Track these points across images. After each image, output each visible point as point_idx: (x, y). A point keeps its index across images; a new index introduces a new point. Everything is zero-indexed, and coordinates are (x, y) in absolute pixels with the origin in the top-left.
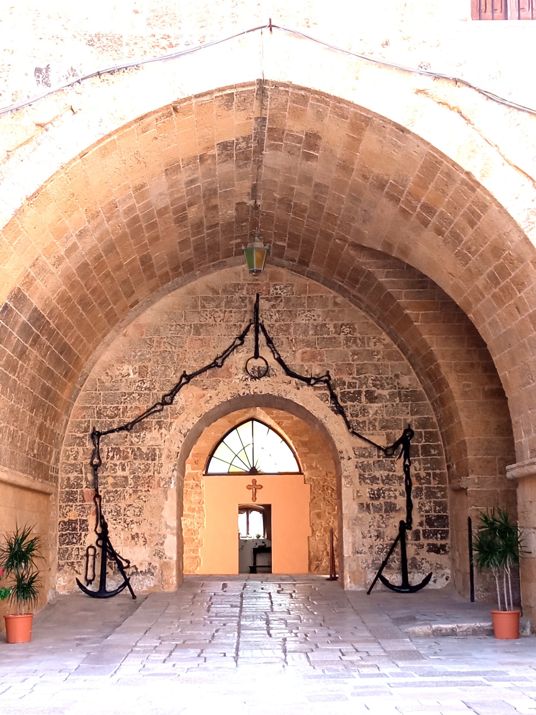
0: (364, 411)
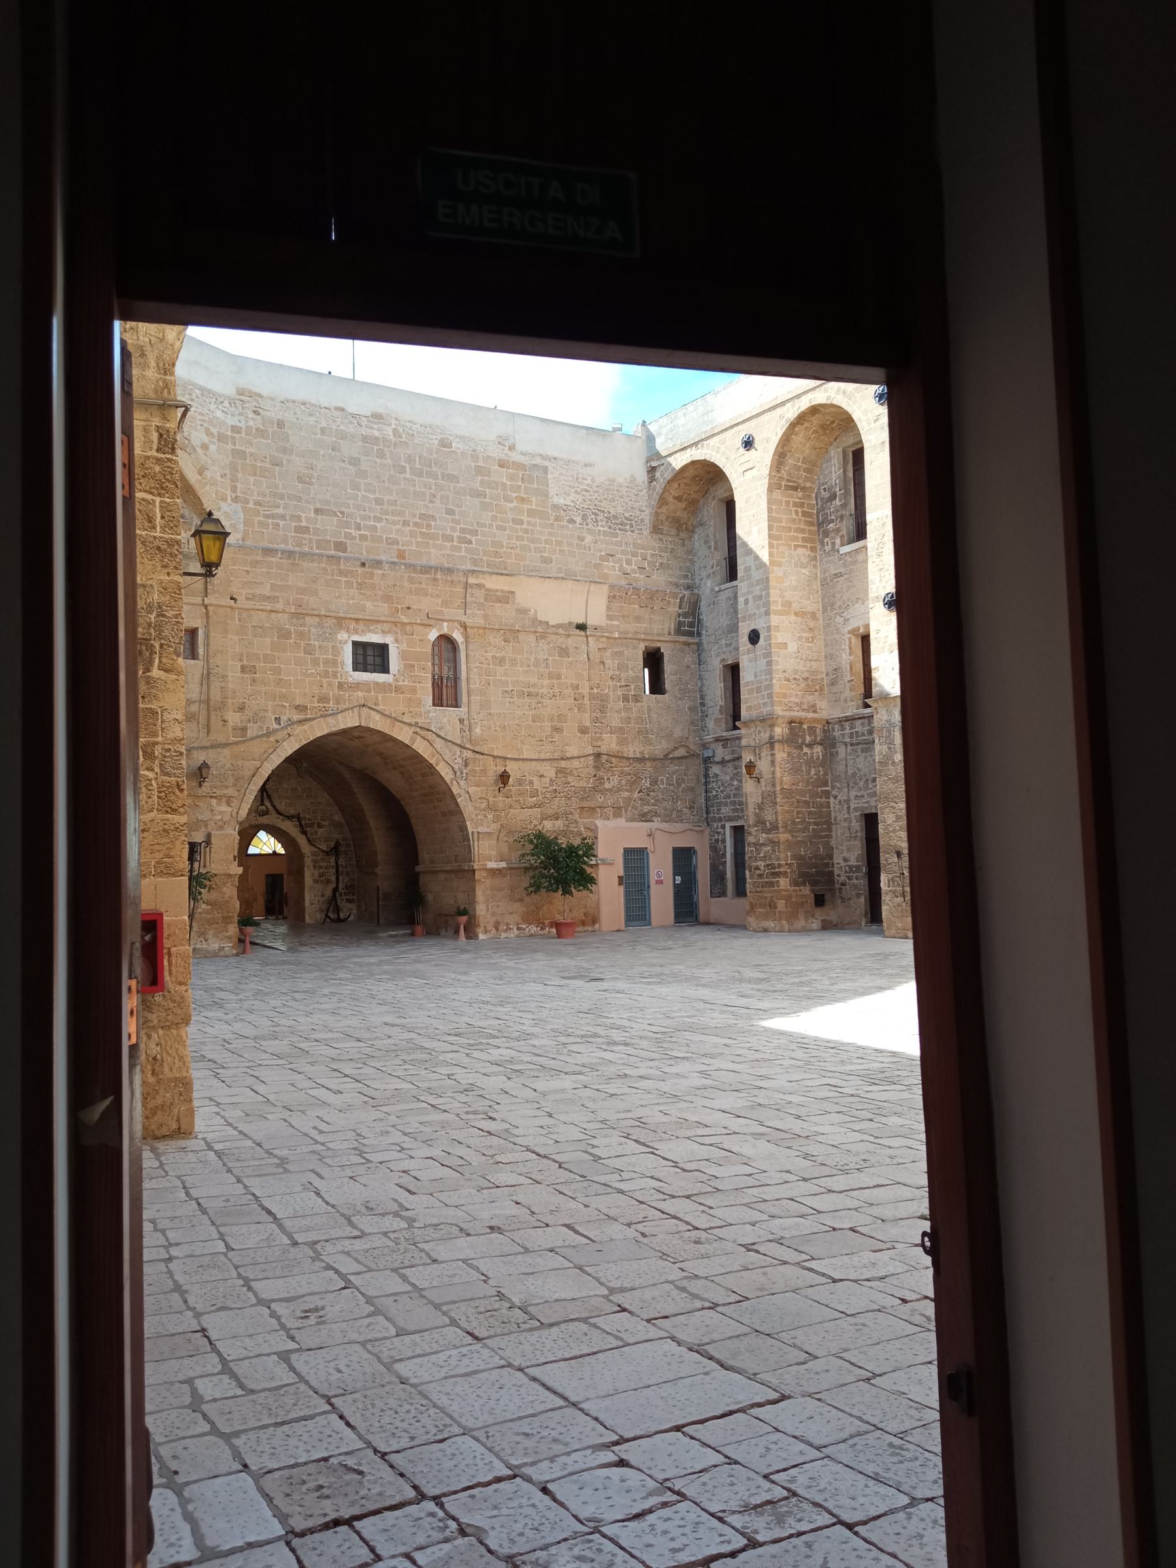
0: (316, 833)
